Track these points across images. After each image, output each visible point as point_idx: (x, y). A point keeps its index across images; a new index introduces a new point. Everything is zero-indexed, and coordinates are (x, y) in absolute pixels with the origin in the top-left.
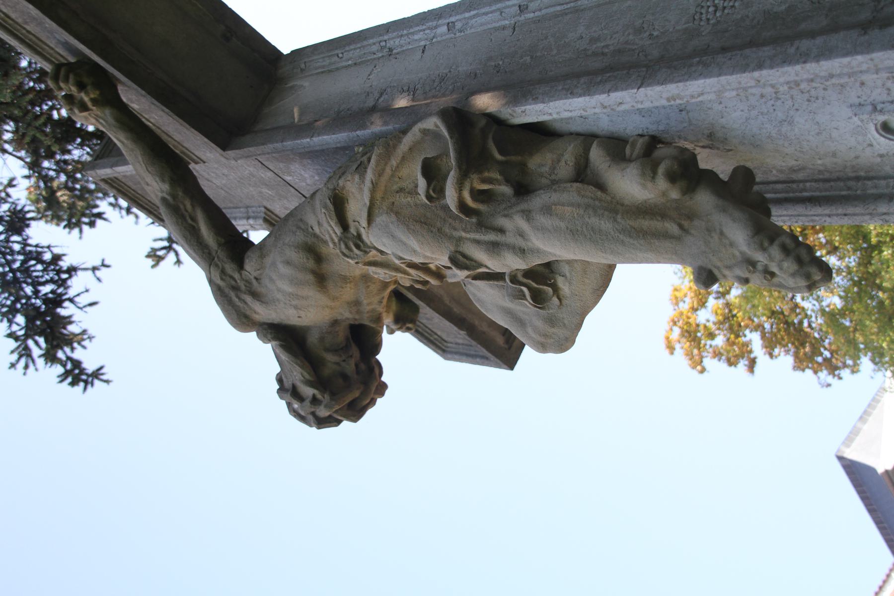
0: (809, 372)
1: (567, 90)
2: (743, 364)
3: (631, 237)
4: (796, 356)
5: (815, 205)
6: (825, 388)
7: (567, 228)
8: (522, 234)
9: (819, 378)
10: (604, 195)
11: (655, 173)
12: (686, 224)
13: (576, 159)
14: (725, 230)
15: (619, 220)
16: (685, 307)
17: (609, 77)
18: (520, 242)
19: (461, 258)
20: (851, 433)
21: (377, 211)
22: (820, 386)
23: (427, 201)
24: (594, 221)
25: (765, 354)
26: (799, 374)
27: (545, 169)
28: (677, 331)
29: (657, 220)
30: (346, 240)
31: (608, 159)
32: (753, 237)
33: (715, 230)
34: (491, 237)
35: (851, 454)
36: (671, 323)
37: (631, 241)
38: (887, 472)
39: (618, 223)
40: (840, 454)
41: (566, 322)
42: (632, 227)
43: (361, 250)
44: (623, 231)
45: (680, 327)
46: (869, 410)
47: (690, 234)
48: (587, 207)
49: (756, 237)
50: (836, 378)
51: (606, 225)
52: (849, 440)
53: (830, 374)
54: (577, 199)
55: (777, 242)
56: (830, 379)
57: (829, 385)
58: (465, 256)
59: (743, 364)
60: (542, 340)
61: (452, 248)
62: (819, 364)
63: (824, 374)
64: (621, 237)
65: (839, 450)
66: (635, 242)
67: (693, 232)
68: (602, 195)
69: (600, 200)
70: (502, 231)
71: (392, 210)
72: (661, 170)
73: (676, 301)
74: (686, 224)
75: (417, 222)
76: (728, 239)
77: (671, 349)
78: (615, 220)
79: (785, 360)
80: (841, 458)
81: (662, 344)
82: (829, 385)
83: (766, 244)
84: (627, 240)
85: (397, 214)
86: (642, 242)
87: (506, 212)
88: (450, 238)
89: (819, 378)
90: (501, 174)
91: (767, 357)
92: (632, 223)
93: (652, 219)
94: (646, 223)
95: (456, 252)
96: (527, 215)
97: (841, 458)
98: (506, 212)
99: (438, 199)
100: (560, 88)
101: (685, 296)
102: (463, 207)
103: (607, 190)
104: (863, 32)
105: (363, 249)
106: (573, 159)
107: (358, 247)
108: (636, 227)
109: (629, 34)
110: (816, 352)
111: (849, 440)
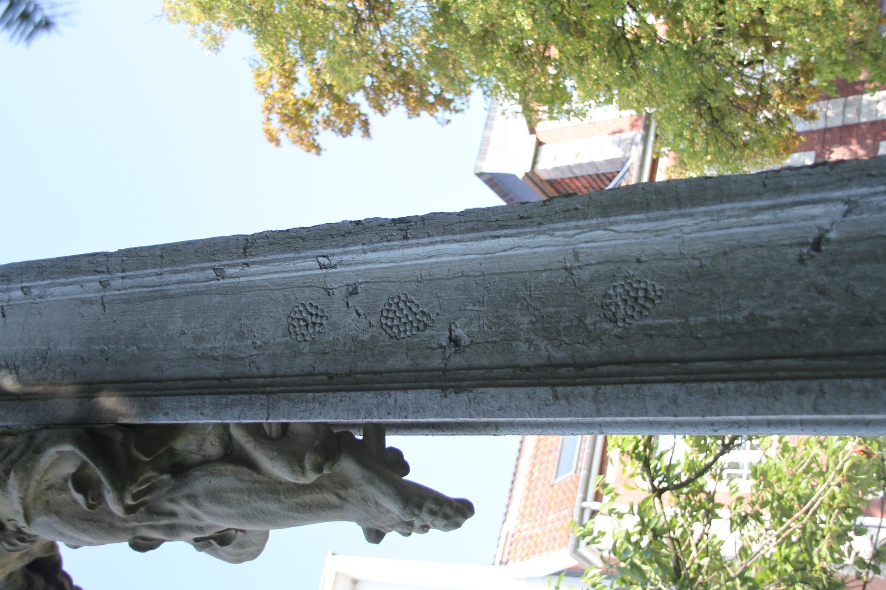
0: (424, 114)
1: (197, 409)
2: (357, 132)
3: (299, 512)
4: (406, 101)
5: (439, 431)
6: (446, 126)
7: (239, 514)
8: (194, 517)
9: (436, 118)
10: (260, 477)
11: (302, 467)
12: (342, 493)
13: (220, 439)
14: (378, 501)
15: (283, 500)
16: (275, 90)
17: (233, 400)
18: (195, 523)
19: (142, 542)
20: (482, 145)
21: (33, 511)
22: (439, 126)
23: (88, 510)
24: (261, 505)
25: (375, 113)
26: (415, 120)
27: (193, 447)
28: (275, 118)
29: (316, 493)
30: (7, 538)
31: (250, 439)
32: (404, 509)
33: (370, 500)
34: (165, 521)
35: (490, 168)
36: (267, 112)
37: (301, 515)
38: (526, 174)
39: (283, 503)
40: (479, 171)
41: (254, 541)
42: (297, 504)
43: (28, 542)
44: (290, 509)
45: (278, 113)
46: (491, 114)
47: (350, 502)
48: (250, 491)
49: (407, 508)
50: (453, 112)
51: (273, 506)
52: (482, 153)
53: (445, 110)
54: (238, 485)
55: (424, 509)
56: (447, 115)
57: (449, 121)
58: (144, 539)
59: (357, 132)
60: (237, 558)
61: (130, 537)
62: (433, 104)
63: (442, 113)
64: (290, 513)
65: (476, 168)
66: (304, 515)
67: (351, 500)
68: (258, 476)
69: (259, 482)
70: (173, 514)
71: (50, 510)
72: (308, 465)
73: (264, 89)
74: (342, 493)
75: (83, 520)
76: (384, 507)
77: (274, 140)
78: (280, 501)
79: (398, 112)
80: (480, 175)
81: (264, 139)
82: (449, 121)
83: (417, 512)
84: (296, 515)
85: (57, 513)
86: (310, 514)
87: (171, 496)
88: (125, 530)
89: (436, 118)
90: (154, 470)
91: (379, 115)
92: (295, 500)
93: (311, 493)
94: (307, 498)
95: (135, 538)
96: (192, 498)
97: (480, 175)
98: (171, 496)
99: (99, 504)
100: (187, 405)
101: (270, 78)
102: (129, 510)
103: (261, 469)
104: (444, 394)
105: (30, 539)
106: (217, 440)
107: (22, 540)
108: (300, 502)
109: (232, 339)
110: (424, 93)
111: (482, 153)
